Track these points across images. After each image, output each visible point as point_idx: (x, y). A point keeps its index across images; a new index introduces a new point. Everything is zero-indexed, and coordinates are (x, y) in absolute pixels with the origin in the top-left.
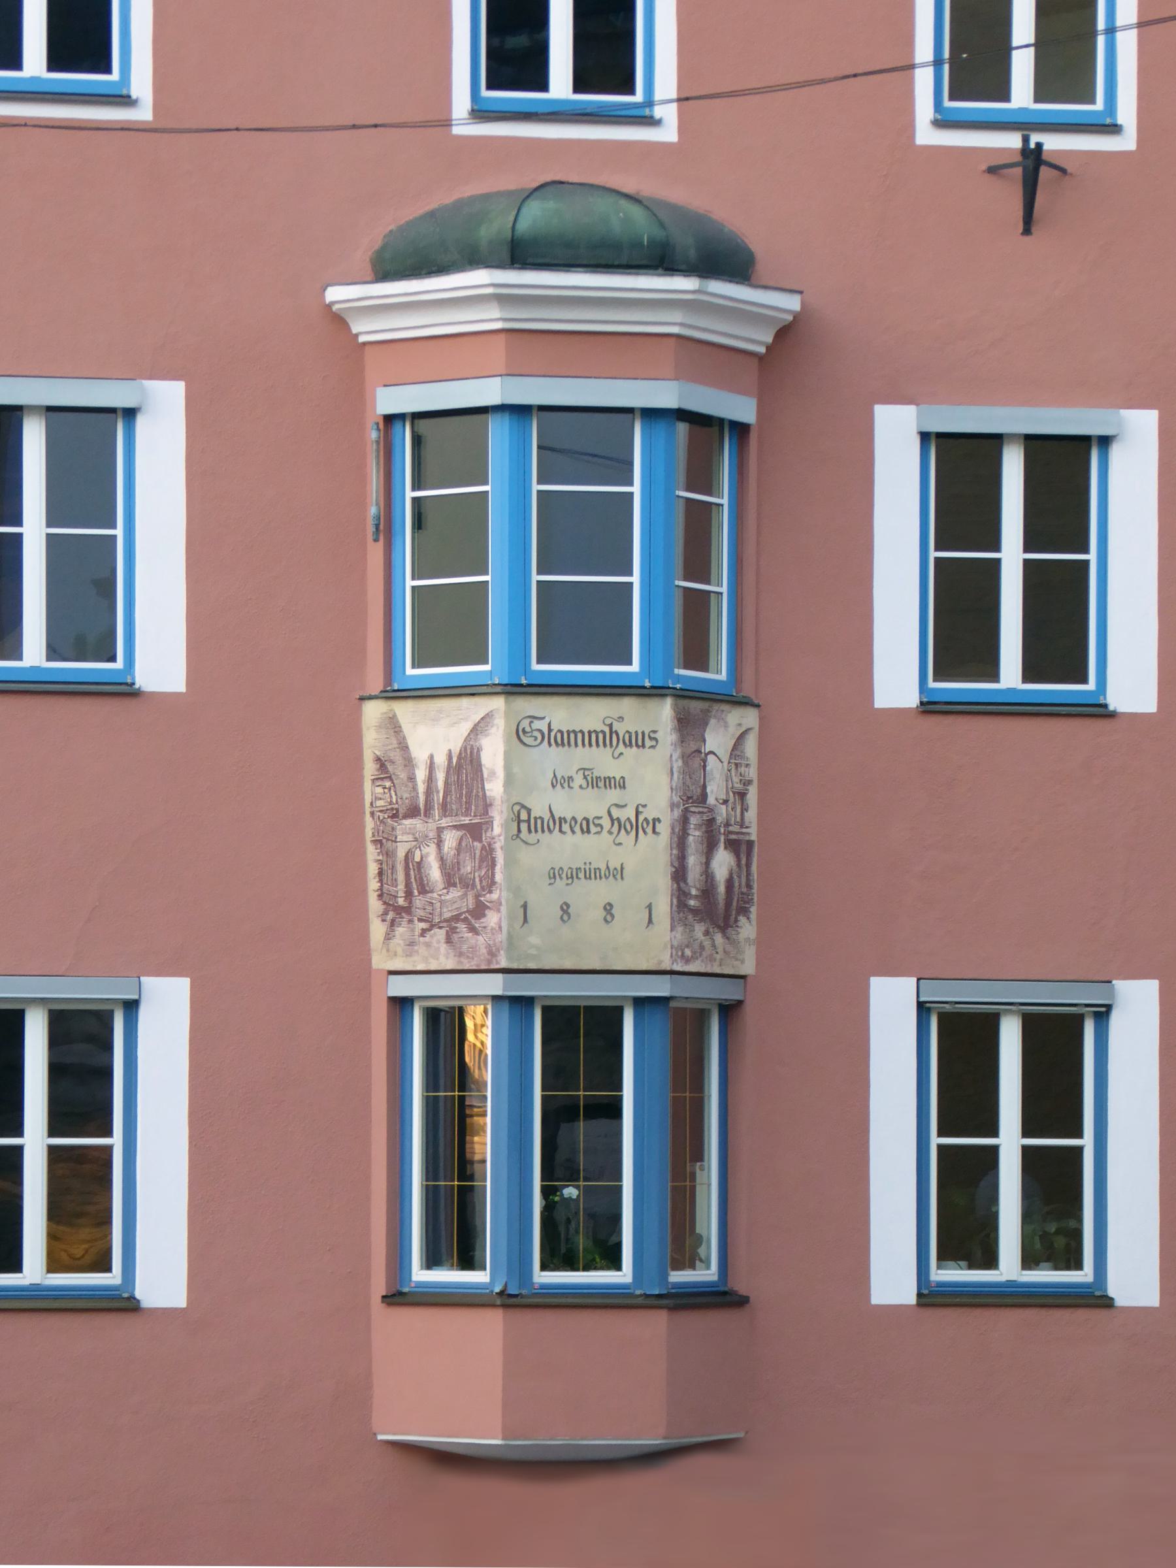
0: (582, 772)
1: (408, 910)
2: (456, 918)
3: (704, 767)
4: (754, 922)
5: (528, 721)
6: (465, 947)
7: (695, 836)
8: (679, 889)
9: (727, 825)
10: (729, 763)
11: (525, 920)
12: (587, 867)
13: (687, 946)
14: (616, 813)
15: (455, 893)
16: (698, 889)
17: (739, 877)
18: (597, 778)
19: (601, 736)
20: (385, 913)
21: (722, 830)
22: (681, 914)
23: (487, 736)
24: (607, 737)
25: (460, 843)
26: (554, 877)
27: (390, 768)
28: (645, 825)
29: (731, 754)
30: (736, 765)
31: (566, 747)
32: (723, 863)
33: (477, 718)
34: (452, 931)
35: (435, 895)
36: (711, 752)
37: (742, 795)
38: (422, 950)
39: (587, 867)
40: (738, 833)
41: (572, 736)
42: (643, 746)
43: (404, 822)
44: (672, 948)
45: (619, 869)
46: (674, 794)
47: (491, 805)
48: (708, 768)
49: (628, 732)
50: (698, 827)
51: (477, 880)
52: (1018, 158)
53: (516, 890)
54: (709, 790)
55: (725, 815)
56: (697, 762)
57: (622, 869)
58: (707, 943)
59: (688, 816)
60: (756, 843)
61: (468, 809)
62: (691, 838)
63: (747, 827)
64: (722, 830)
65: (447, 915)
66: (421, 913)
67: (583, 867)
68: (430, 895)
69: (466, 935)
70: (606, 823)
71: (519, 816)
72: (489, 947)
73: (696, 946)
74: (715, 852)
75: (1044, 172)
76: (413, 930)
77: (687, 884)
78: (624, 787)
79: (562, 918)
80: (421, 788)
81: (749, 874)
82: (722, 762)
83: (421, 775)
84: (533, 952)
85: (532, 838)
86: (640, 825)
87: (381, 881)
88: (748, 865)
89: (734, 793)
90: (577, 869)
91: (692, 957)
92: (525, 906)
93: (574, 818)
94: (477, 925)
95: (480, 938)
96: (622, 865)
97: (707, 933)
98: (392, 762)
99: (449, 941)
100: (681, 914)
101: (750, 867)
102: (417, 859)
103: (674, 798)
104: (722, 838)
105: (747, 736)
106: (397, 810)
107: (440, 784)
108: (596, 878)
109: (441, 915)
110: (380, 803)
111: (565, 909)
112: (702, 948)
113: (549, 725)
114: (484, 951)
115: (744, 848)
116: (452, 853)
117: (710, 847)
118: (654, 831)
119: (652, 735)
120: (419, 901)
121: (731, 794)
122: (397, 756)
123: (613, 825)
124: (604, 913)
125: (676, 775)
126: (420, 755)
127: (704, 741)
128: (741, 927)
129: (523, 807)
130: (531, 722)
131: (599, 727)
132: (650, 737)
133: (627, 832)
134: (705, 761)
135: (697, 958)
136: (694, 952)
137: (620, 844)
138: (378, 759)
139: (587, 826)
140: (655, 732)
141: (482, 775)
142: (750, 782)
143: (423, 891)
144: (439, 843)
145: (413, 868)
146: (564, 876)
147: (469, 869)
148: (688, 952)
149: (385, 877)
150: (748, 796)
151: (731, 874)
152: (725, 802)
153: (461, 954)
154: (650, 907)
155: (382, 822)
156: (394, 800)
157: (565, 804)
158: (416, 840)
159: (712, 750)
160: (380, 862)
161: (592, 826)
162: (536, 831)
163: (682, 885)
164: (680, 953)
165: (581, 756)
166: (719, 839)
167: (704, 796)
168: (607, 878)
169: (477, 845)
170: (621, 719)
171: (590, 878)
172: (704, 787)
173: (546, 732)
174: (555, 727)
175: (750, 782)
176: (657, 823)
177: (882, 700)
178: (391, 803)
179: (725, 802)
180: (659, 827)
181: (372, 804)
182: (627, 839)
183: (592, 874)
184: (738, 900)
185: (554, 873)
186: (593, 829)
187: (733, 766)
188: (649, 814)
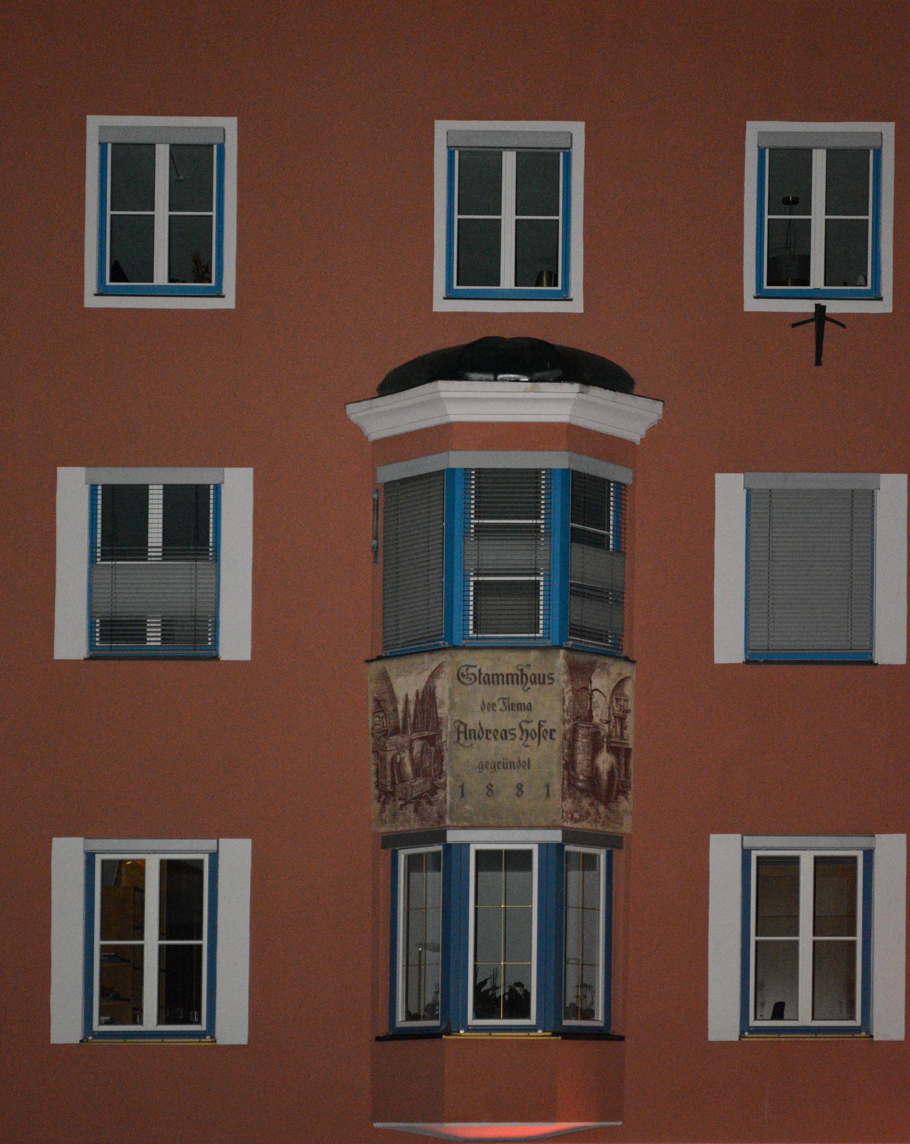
0: (502, 700)
1: (393, 794)
2: (420, 796)
3: (591, 699)
4: (631, 801)
5: (465, 668)
6: (425, 814)
7: (582, 742)
8: (569, 774)
9: (609, 736)
10: (611, 698)
11: (463, 795)
12: (505, 761)
13: (576, 811)
14: (525, 726)
15: (420, 781)
16: (585, 776)
17: (619, 771)
18: (512, 704)
19: (515, 677)
20: (380, 797)
21: (605, 740)
22: (571, 791)
23: (439, 679)
24: (519, 678)
25: (422, 749)
26: (482, 768)
27: (383, 704)
28: (545, 734)
29: (613, 692)
30: (617, 700)
31: (491, 685)
32: (605, 761)
33: (434, 668)
34: (418, 804)
35: (408, 783)
36: (596, 690)
37: (622, 719)
38: (401, 818)
39: (505, 761)
40: (617, 743)
41: (495, 677)
42: (544, 683)
43: (392, 738)
44: (563, 812)
45: (527, 762)
46: (565, 714)
47: (441, 722)
48: (593, 700)
49: (533, 674)
50: (585, 736)
51: (433, 770)
52: (813, 316)
53: (457, 777)
54: (594, 713)
55: (607, 730)
56: (585, 695)
57: (529, 762)
58: (592, 811)
59: (578, 729)
60: (633, 751)
61: (428, 726)
62: (579, 743)
63: (625, 740)
64: (605, 740)
65: (414, 795)
66: (400, 795)
67: (502, 761)
68: (405, 783)
69: (426, 806)
70: (518, 732)
71: (459, 728)
72: (439, 812)
73: (583, 812)
74: (599, 753)
75: (828, 324)
76: (395, 806)
77: (575, 771)
78: (531, 710)
79: (487, 793)
80: (401, 715)
81: (627, 769)
82: (605, 697)
83: (400, 707)
84: (468, 815)
85: (468, 743)
86: (542, 733)
87: (377, 777)
88: (627, 764)
89: (615, 717)
90: (498, 763)
91: (579, 819)
92: (462, 787)
93: (496, 730)
94: (432, 800)
95: (434, 808)
96: (529, 759)
97: (592, 804)
98: (385, 701)
99: (416, 811)
100: (571, 791)
101: (628, 765)
102: (398, 761)
103: (566, 716)
104: (605, 745)
105: (626, 682)
106: (387, 730)
107: (412, 712)
108: (511, 768)
109: (411, 795)
110: (378, 727)
111: (490, 788)
112: (588, 813)
113: (480, 671)
114: (436, 816)
115: (622, 753)
116: (418, 755)
117: (595, 749)
118: (551, 738)
119: (550, 676)
120: (399, 787)
121: (613, 718)
122: (387, 697)
123: (523, 733)
124: (517, 790)
125: (567, 703)
126: (400, 694)
127: (591, 682)
128: (620, 803)
129: (462, 723)
130: (468, 669)
131: (514, 671)
132: (548, 677)
133: (533, 738)
134: (591, 695)
135: (584, 820)
136: (581, 816)
137: (527, 746)
138: (377, 701)
139: (505, 735)
140: (552, 674)
141: (436, 704)
142: (628, 711)
143: (402, 781)
144: (411, 751)
145: (397, 765)
146: (489, 767)
147: (428, 764)
148: (576, 815)
149: (380, 774)
150: (627, 720)
151: (612, 768)
152: (608, 722)
153: (423, 819)
154: (548, 786)
155: (378, 739)
156: (385, 725)
157: (489, 720)
158: (397, 748)
159: (597, 687)
160: (377, 765)
161: (508, 735)
162: (470, 738)
163: (572, 773)
164: (570, 816)
165: (501, 690)
166: (603, 746)
167: (591, 717)
168: (519, 768)
169: (433, 749)
170: (529, 666)
171: (507, 768)
172: (591, 711)
173: (477, 675)
174: (484, 671)
175: (628, 711)
176: (553, 732)
177: (721, 657)
178: (383, 727)
179: (608, 722)
180: (555, 735)
181: (372, 728)
182: (533, 743)
183: (509, 765)
184: (618, 786)
185: (482, 765)
186: (509, 737)
187: (614, 699)
188: (548, 726)
